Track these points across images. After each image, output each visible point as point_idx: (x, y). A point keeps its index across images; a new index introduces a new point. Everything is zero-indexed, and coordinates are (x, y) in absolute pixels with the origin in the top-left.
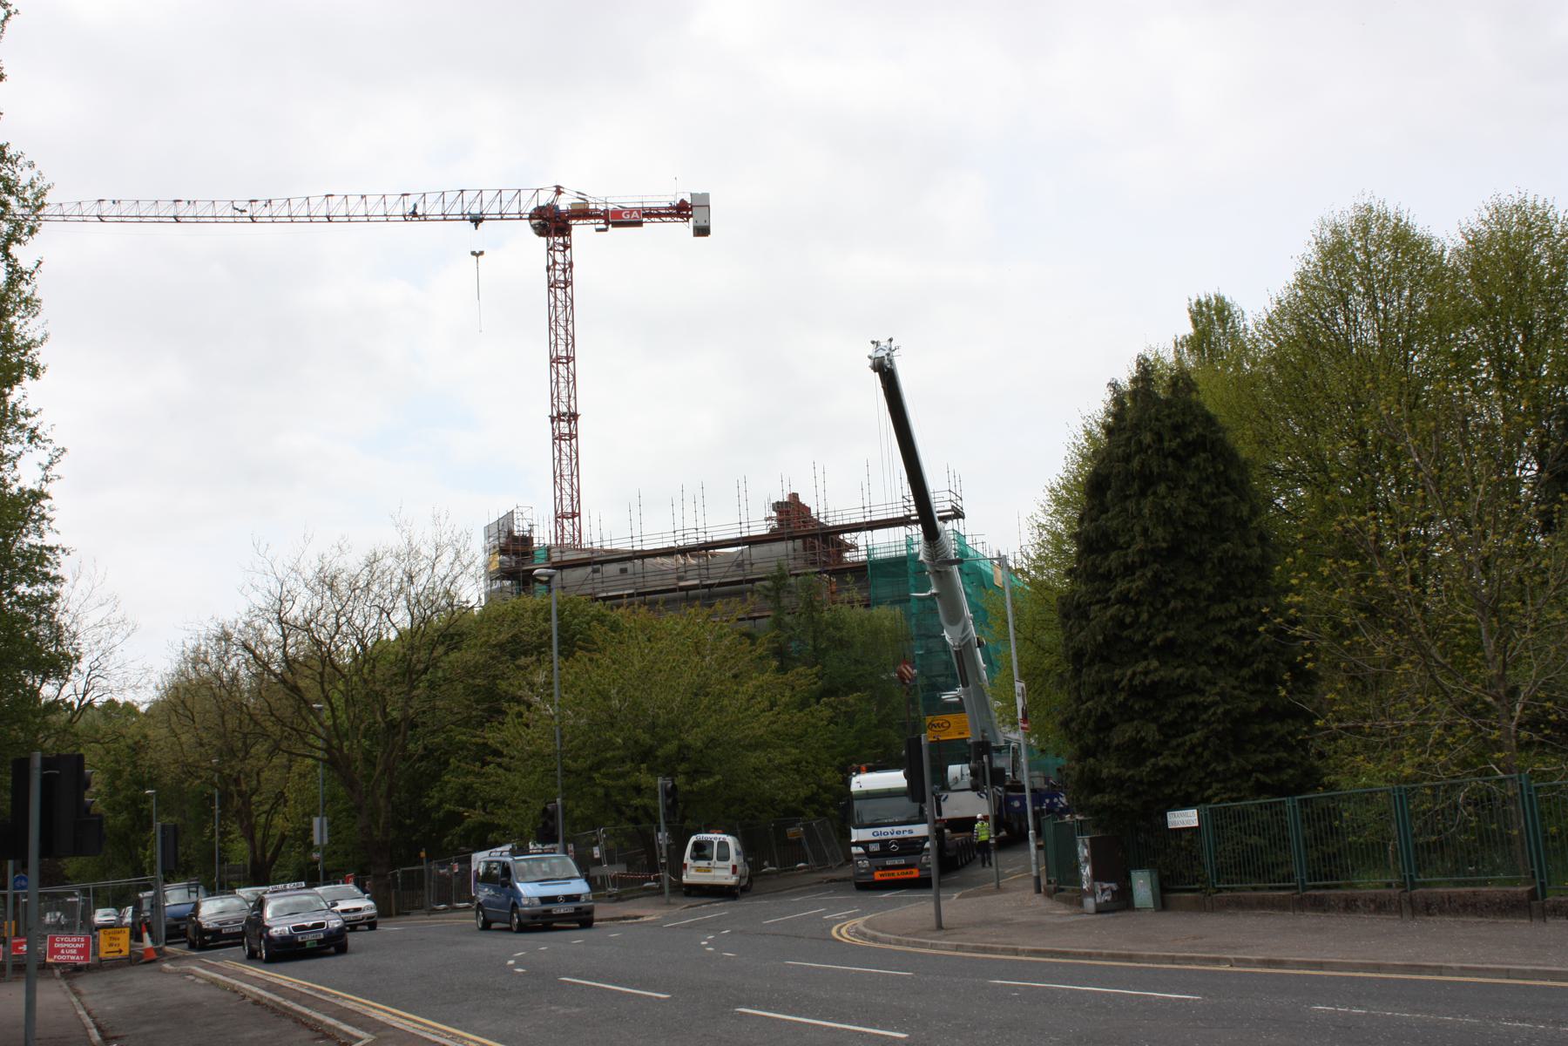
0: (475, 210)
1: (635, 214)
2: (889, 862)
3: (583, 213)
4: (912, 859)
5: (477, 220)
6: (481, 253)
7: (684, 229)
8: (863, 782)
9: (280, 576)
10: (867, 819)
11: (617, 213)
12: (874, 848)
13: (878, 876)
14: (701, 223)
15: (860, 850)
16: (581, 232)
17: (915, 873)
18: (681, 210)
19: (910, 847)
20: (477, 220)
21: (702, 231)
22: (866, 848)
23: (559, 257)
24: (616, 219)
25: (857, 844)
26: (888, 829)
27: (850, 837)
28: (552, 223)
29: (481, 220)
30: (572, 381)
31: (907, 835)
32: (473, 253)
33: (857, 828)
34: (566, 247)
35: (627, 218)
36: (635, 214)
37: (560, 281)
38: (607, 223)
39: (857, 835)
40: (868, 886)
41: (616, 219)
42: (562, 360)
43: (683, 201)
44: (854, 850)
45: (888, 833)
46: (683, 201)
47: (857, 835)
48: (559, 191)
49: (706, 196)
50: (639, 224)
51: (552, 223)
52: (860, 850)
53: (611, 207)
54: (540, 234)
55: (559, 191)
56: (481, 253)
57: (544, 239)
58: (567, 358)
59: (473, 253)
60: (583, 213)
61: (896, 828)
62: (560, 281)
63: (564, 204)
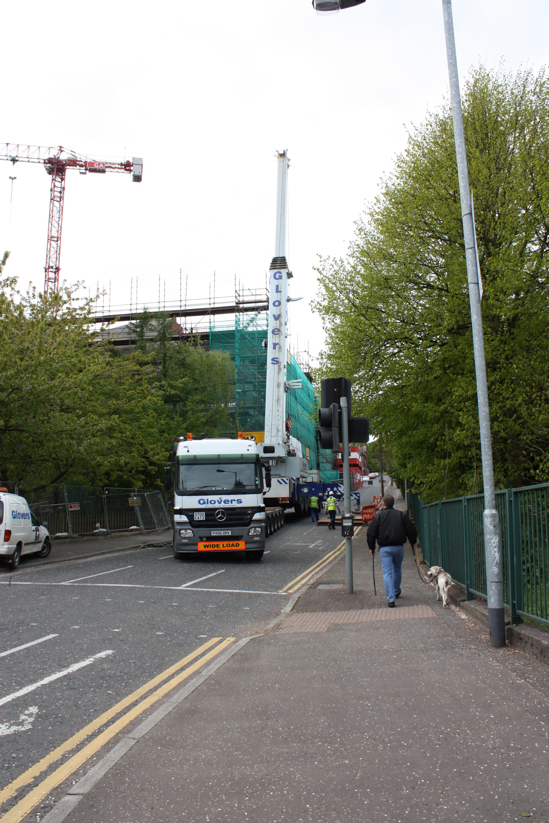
0: (14, 155)
1: (101, 165)
2: (214, 533)
3: (73, 163)
4: (238, 531)
5: (14, 160)
6: (15, 178)
7: (129, 177)
8: (188, 448)
9: (229, 486)
10: (191, 485)
11: (91, 164)
12: (200, 517)
13: (201, 547)
14: (137, 173)
15: (184, 518)
16: (71, 172)
17: (242, 546)
18: (127, 166)
19: (239, 517)
20: (14, 160)
21: (137, 179)
22: (190, 517)
23: (57, 184)
24: (93, 168)
25: (181, 512)
26: (216, 498)
27: (173, 504)
28: (57, 167)
29: (17, 161)
30: (58, 252)
31: (235, 505)
32: (10, 178)
33: (182, 494)
34: (63, 179)
35: (97, 167)
36: (101, 165)
37: (58, 197)
38: (86, 169)
39: (181, 502)
40: (189, 557)
41: (93, 168)
42: (54, 239)
43: (128, 162)
44: (178, 518)
45: (217, 502)
46: (128, 162)
47: (181, 502)
48: (61, 150)
49: (141, 159)
50: (103, 171)
51: (57, 167)
52: (184, 518)
53: (88, 161)
54: (50, 173)
55: (61, 150)
56: (15, 178)
57: (51, 176)
58: (58, 238)
59: (10, 178)
60: (73, 163)
61: (224, 497)
62: (58, 197)
63: (64, 157)
